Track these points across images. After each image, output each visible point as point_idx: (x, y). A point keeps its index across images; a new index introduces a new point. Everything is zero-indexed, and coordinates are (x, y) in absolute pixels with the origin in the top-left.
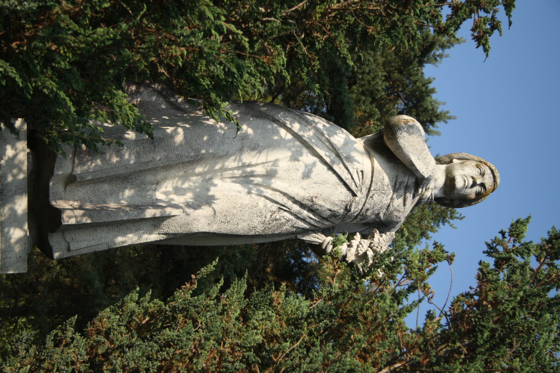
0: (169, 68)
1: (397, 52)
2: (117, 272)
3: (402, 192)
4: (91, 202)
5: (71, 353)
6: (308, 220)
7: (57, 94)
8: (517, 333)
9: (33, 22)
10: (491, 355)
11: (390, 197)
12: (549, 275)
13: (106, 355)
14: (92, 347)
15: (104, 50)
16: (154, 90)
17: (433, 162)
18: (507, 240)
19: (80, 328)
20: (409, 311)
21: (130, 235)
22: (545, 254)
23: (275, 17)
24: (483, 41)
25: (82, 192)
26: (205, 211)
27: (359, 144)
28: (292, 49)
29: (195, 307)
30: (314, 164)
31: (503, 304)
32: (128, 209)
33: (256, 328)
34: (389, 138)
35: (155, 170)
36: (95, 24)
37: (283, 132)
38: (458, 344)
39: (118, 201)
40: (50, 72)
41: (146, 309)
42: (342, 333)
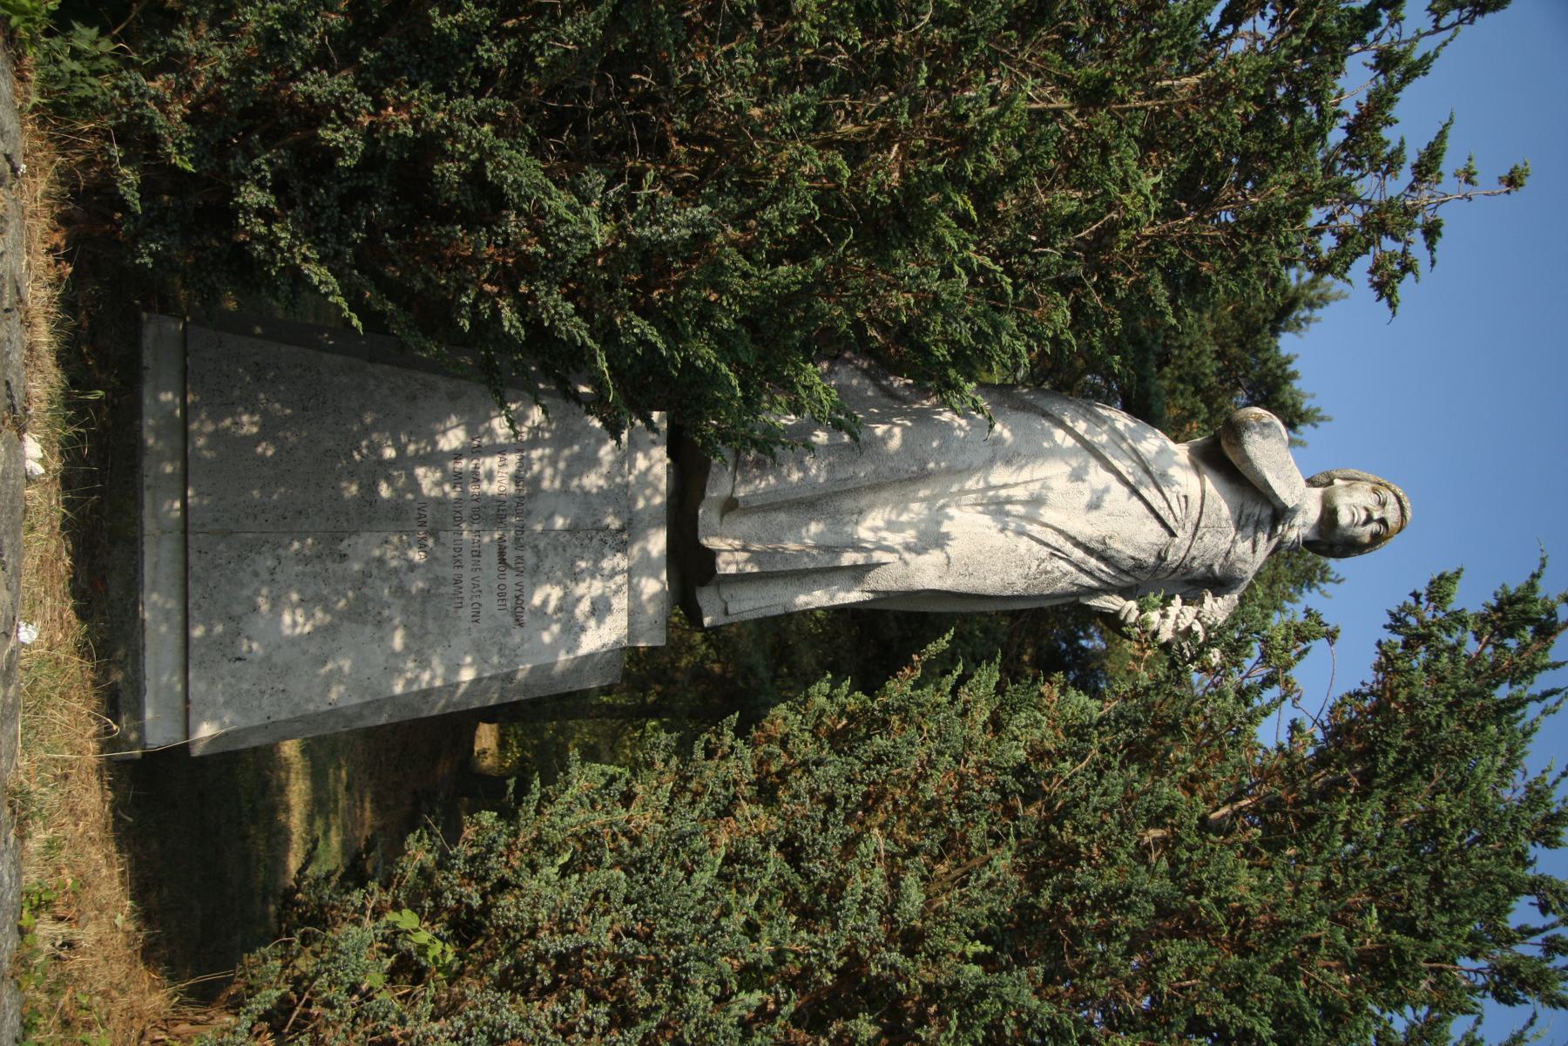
0: (884, 329)
1: (1236, 314)
2: (786, 653)
3: (1250, 530)
4: (760, 540)
5: (731, 768)
6: (1097, 573)
7: (716, 368)
8: (1444, 755)
9: (685, 260)
10: (1397, 790)
11: (1230, 538)
12: (1495, 665)
13: (782, 774)
14: (761, 763)
15: (788, 300)
16: (857, 368)
17: (1302, 483)
18: (1422, 607)
19: (741, 732)
20: (1265, 715)
21: (818, 593)
22: (1489, 628)
23: (1052, 247)
24: (1388, 290)
25: (746, 525)
26: (934, 557)
27: (1181, 451)
28: (1077, 299)
29: (919, 705)
30: (1107, 490)
31: (1423, 708)
32: (815, 552)
33: (1016, 738)
34: (1230, 444)
35: (856, 491)
36: (775, 261)
37: (1059, 434)
38: (1346, 770)
39: (800, 540)
40: (706, 336)
41: (843, 707)
42: (1154, 751)
